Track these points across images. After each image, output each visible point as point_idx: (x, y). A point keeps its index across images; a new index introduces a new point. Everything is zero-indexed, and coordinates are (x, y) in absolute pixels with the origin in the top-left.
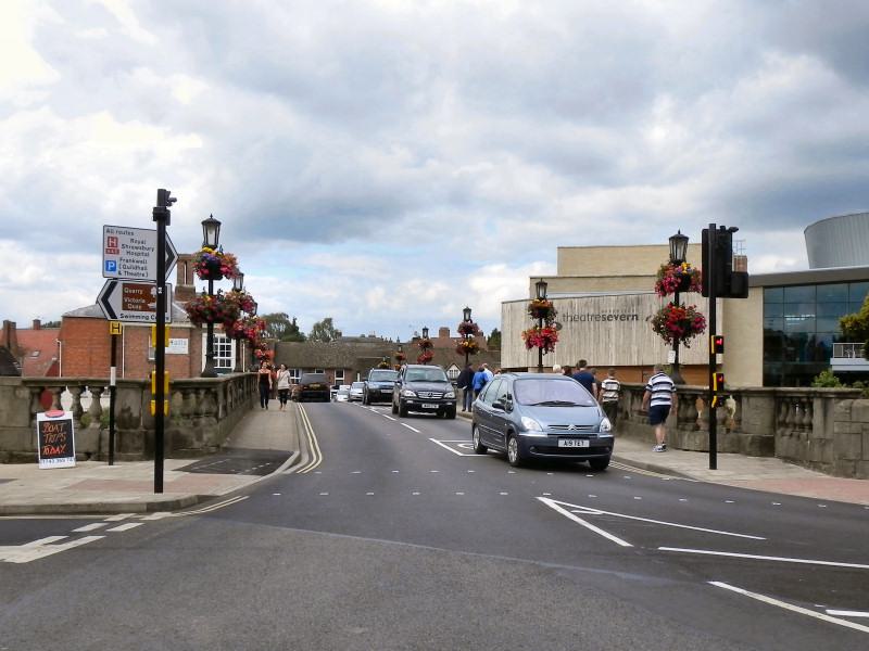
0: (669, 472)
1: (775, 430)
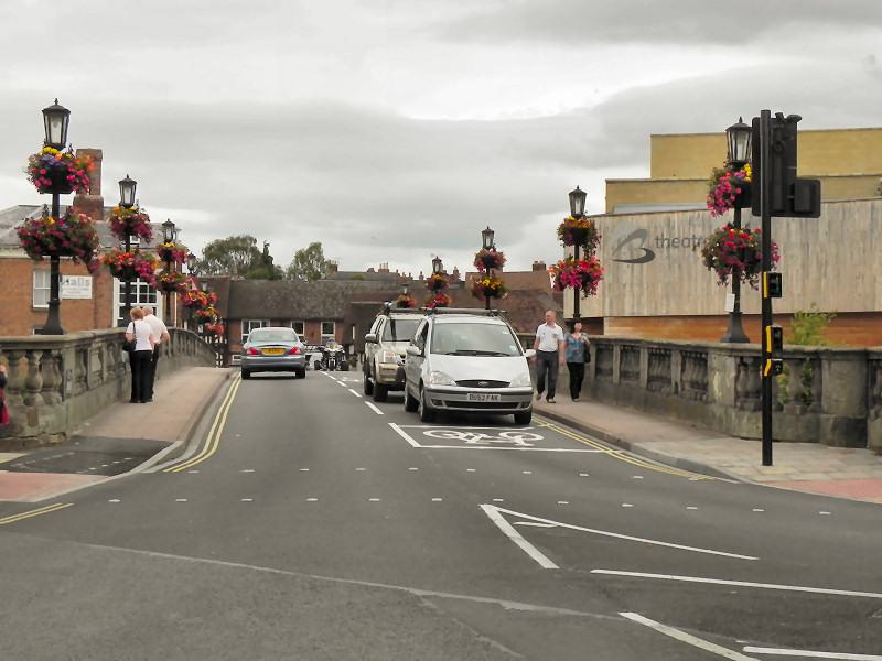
0: (706, 470)
1: (867, 408)
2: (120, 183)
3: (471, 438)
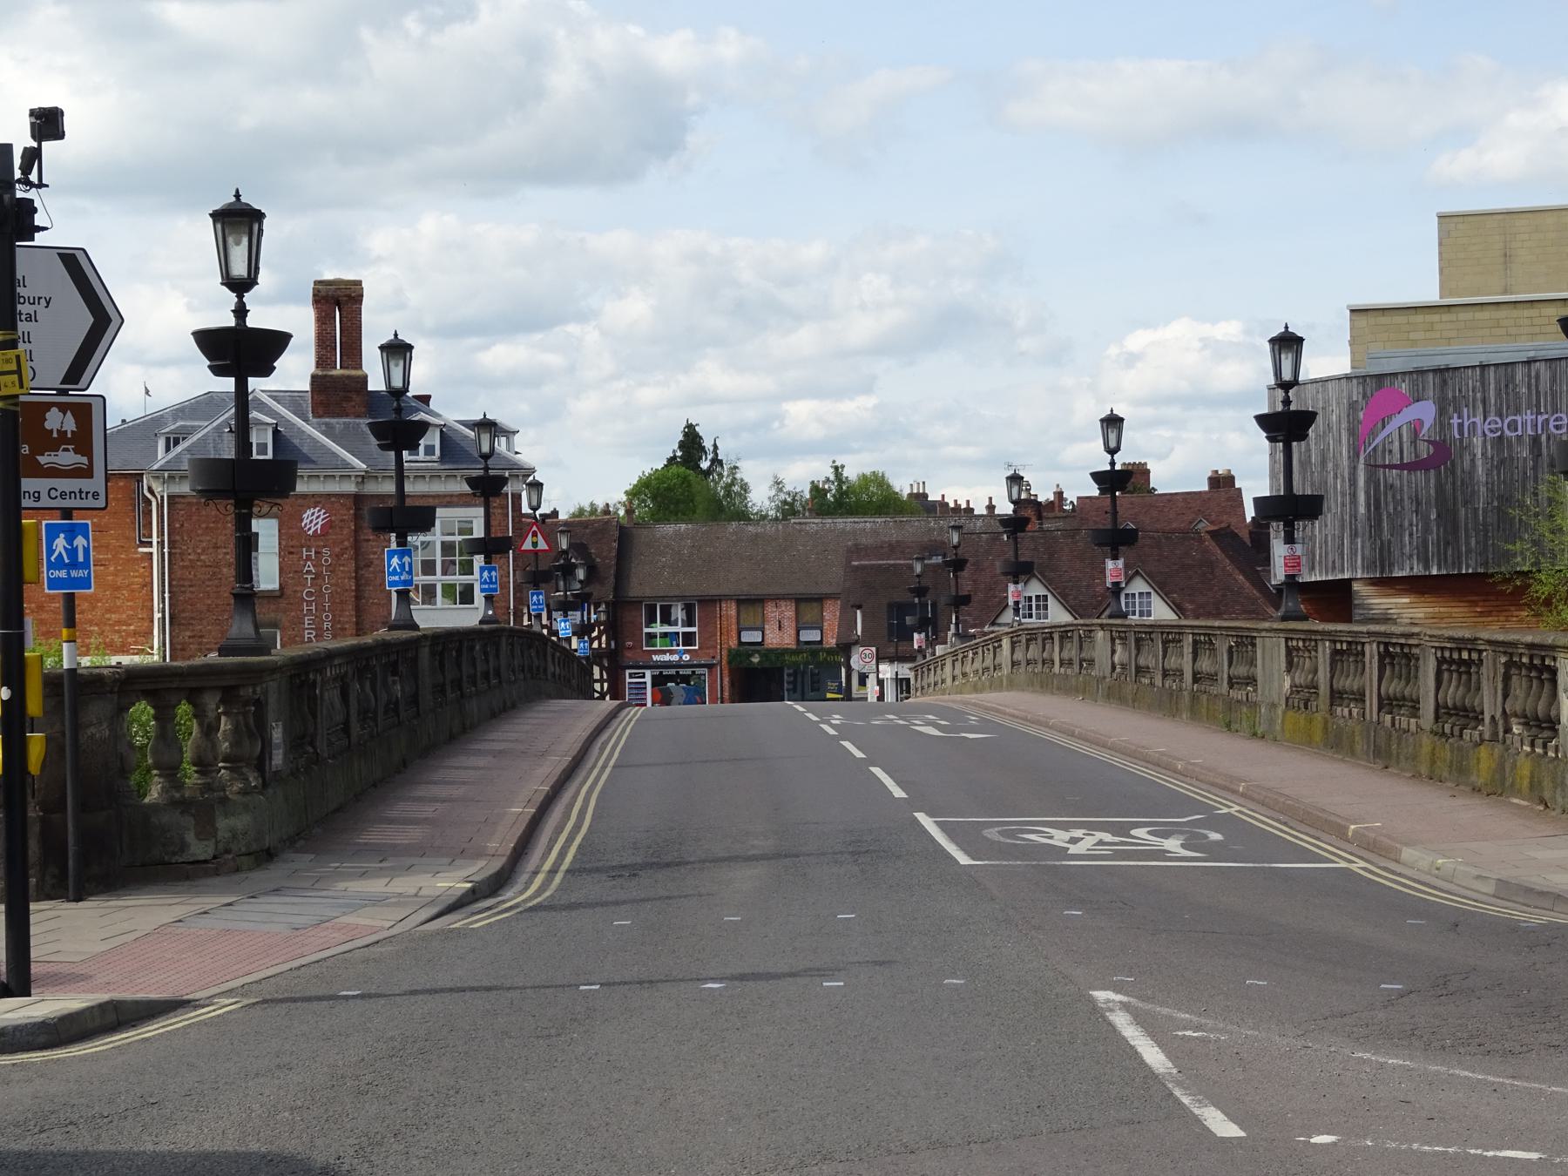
2: (382, 348)
3: (1074, 841)
